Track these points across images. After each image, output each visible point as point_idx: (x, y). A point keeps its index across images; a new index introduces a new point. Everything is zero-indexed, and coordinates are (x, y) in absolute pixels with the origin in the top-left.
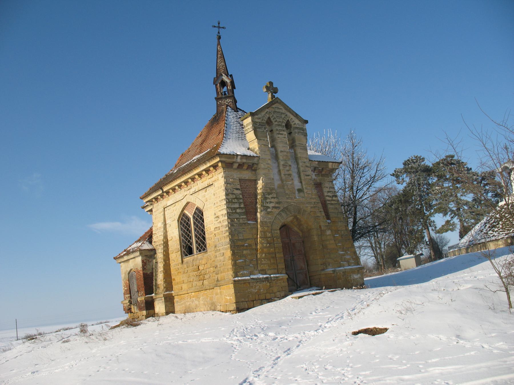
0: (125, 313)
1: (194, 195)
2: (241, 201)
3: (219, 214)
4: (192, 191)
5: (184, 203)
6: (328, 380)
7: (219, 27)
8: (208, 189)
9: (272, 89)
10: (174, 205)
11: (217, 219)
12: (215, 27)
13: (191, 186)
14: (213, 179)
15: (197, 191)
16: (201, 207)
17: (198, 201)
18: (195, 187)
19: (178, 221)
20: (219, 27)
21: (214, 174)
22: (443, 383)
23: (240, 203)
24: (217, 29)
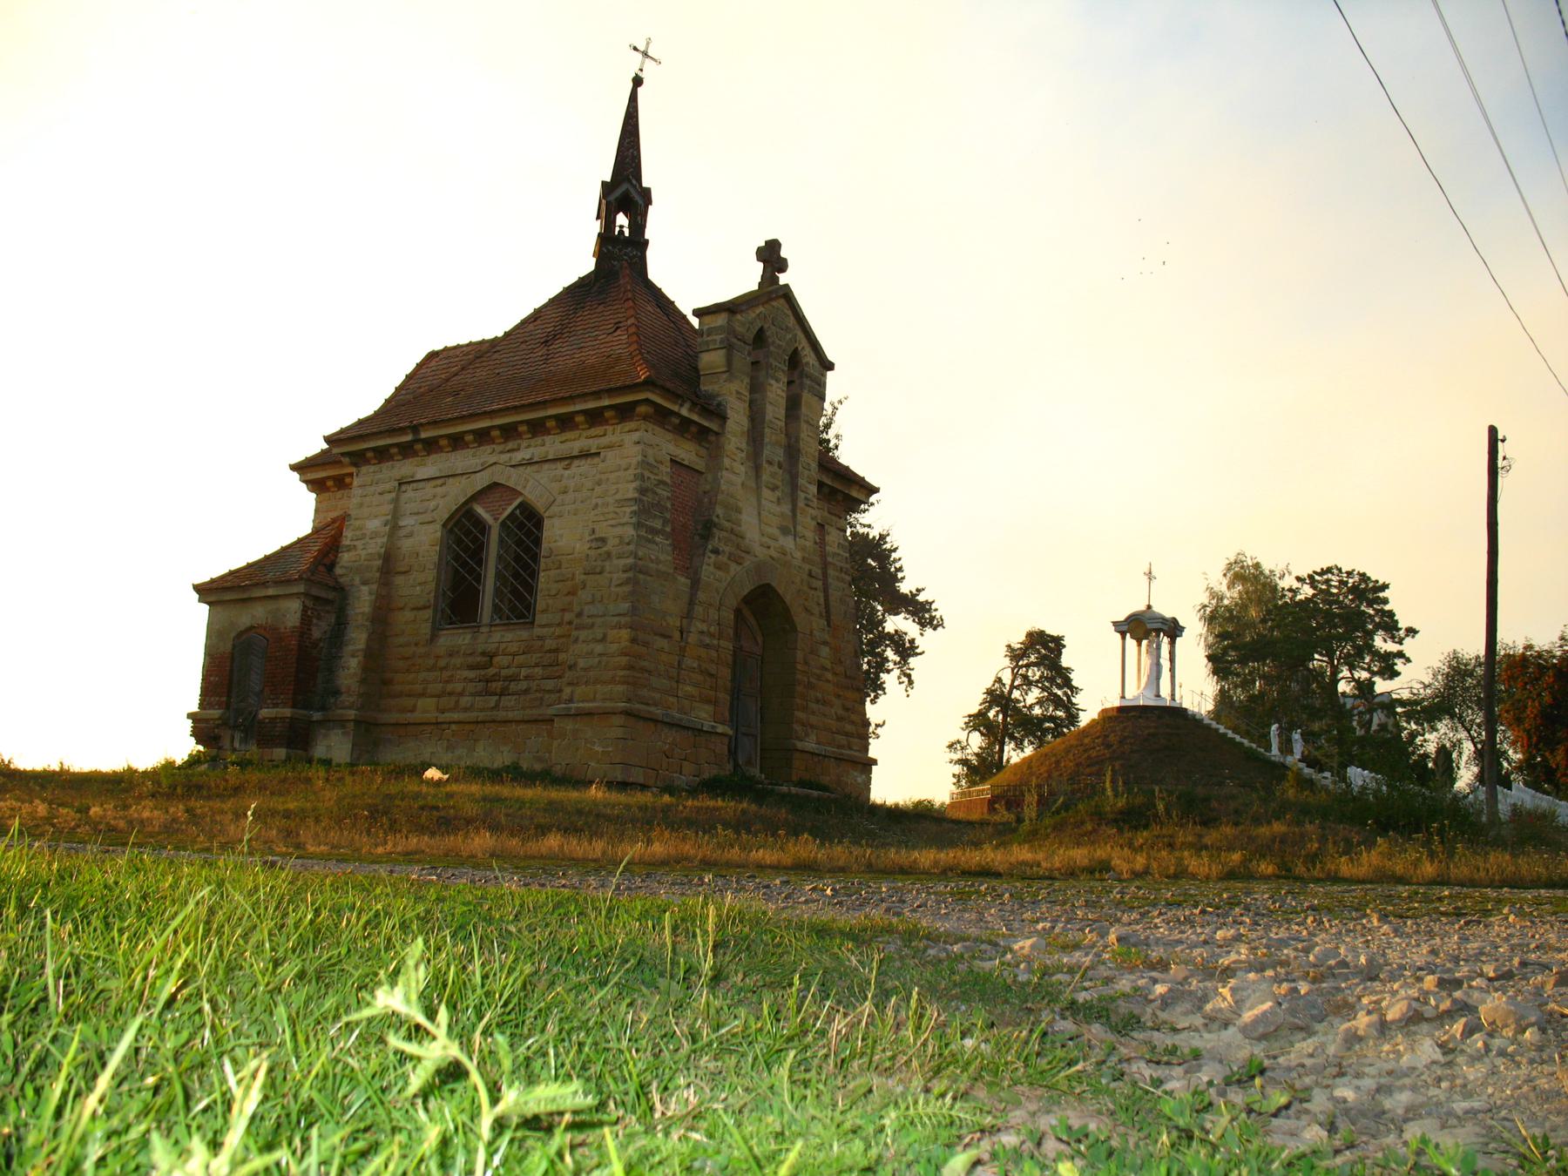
0: (190, 716)
1: (521, 468)
2: (668, 516)
3: (611, 534)
4: (518, 457)
5: (481, 481)
6: (1454, 1001)
7: (645, 54)
8: (576, 462)
9: (771, 256)
10: (439, 482)
11: (599, 544)
12: (635, 49)
13: (519, 445)
14: (604, 441)
15: (550, 457)
16: (539, 505)
17: (535, 487)
18: (531, 450)
19: (444, 526)
20: (645, 54)
21: (610, 428)
22: (6, 1130)
23: (666, 521)
24: (639, 56)
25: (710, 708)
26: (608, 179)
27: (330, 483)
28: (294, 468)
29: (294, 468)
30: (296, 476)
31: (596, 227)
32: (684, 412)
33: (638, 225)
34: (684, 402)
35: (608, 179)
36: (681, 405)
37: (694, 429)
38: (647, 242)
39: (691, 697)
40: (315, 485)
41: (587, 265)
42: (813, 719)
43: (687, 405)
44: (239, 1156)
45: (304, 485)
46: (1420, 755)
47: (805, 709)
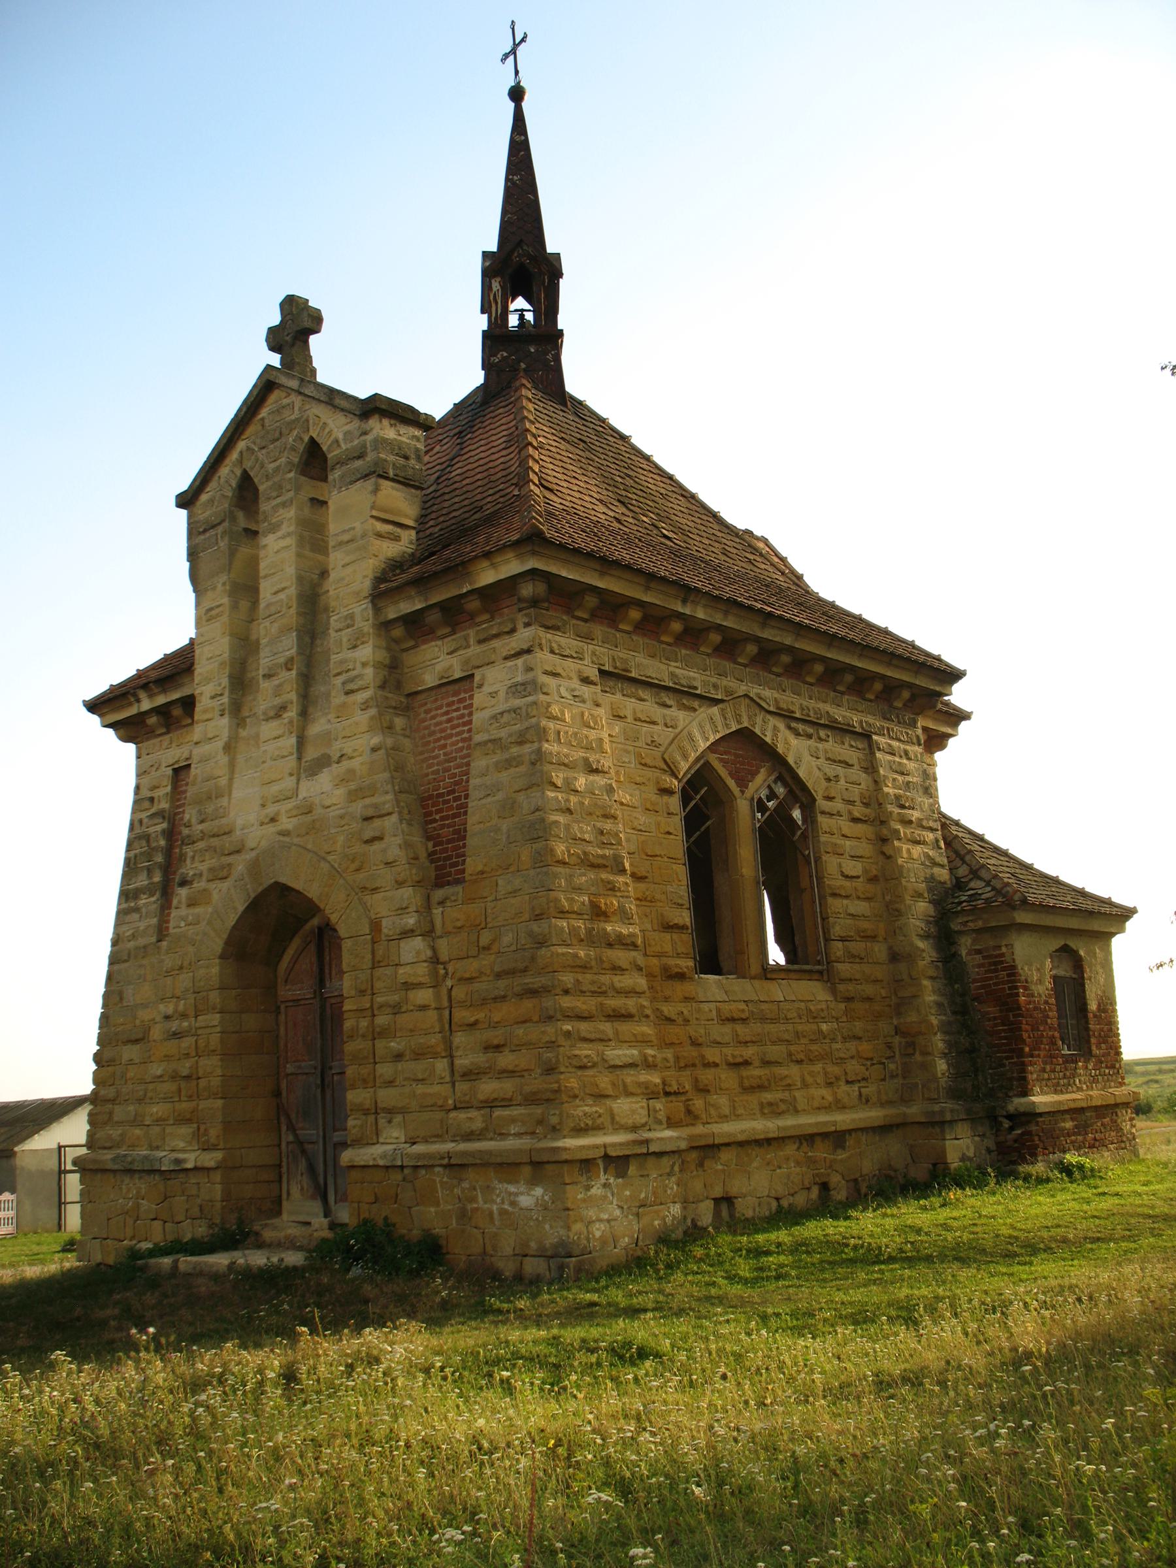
25: (186, 1130)
26: (493, 247)
27: (152, 720)
28: (93, 706)
29: (93, 706)
30: (95, 719)
31: (482, 322)
32: (146, 705)
33: (548, 306)
34: (135, 695)
35: (493, 247)
36: (138, 701)
37: (591, 601)
38: (560, 334)
39: (159, 1121)
40: (128, 730)
41: (476, 377)
42: (387, 1097)
43: (142, 695)
44: (956, 845)
45: (110, 732)
46: (1037, 1146)
47: (369, 1082)
